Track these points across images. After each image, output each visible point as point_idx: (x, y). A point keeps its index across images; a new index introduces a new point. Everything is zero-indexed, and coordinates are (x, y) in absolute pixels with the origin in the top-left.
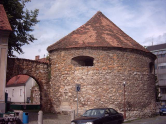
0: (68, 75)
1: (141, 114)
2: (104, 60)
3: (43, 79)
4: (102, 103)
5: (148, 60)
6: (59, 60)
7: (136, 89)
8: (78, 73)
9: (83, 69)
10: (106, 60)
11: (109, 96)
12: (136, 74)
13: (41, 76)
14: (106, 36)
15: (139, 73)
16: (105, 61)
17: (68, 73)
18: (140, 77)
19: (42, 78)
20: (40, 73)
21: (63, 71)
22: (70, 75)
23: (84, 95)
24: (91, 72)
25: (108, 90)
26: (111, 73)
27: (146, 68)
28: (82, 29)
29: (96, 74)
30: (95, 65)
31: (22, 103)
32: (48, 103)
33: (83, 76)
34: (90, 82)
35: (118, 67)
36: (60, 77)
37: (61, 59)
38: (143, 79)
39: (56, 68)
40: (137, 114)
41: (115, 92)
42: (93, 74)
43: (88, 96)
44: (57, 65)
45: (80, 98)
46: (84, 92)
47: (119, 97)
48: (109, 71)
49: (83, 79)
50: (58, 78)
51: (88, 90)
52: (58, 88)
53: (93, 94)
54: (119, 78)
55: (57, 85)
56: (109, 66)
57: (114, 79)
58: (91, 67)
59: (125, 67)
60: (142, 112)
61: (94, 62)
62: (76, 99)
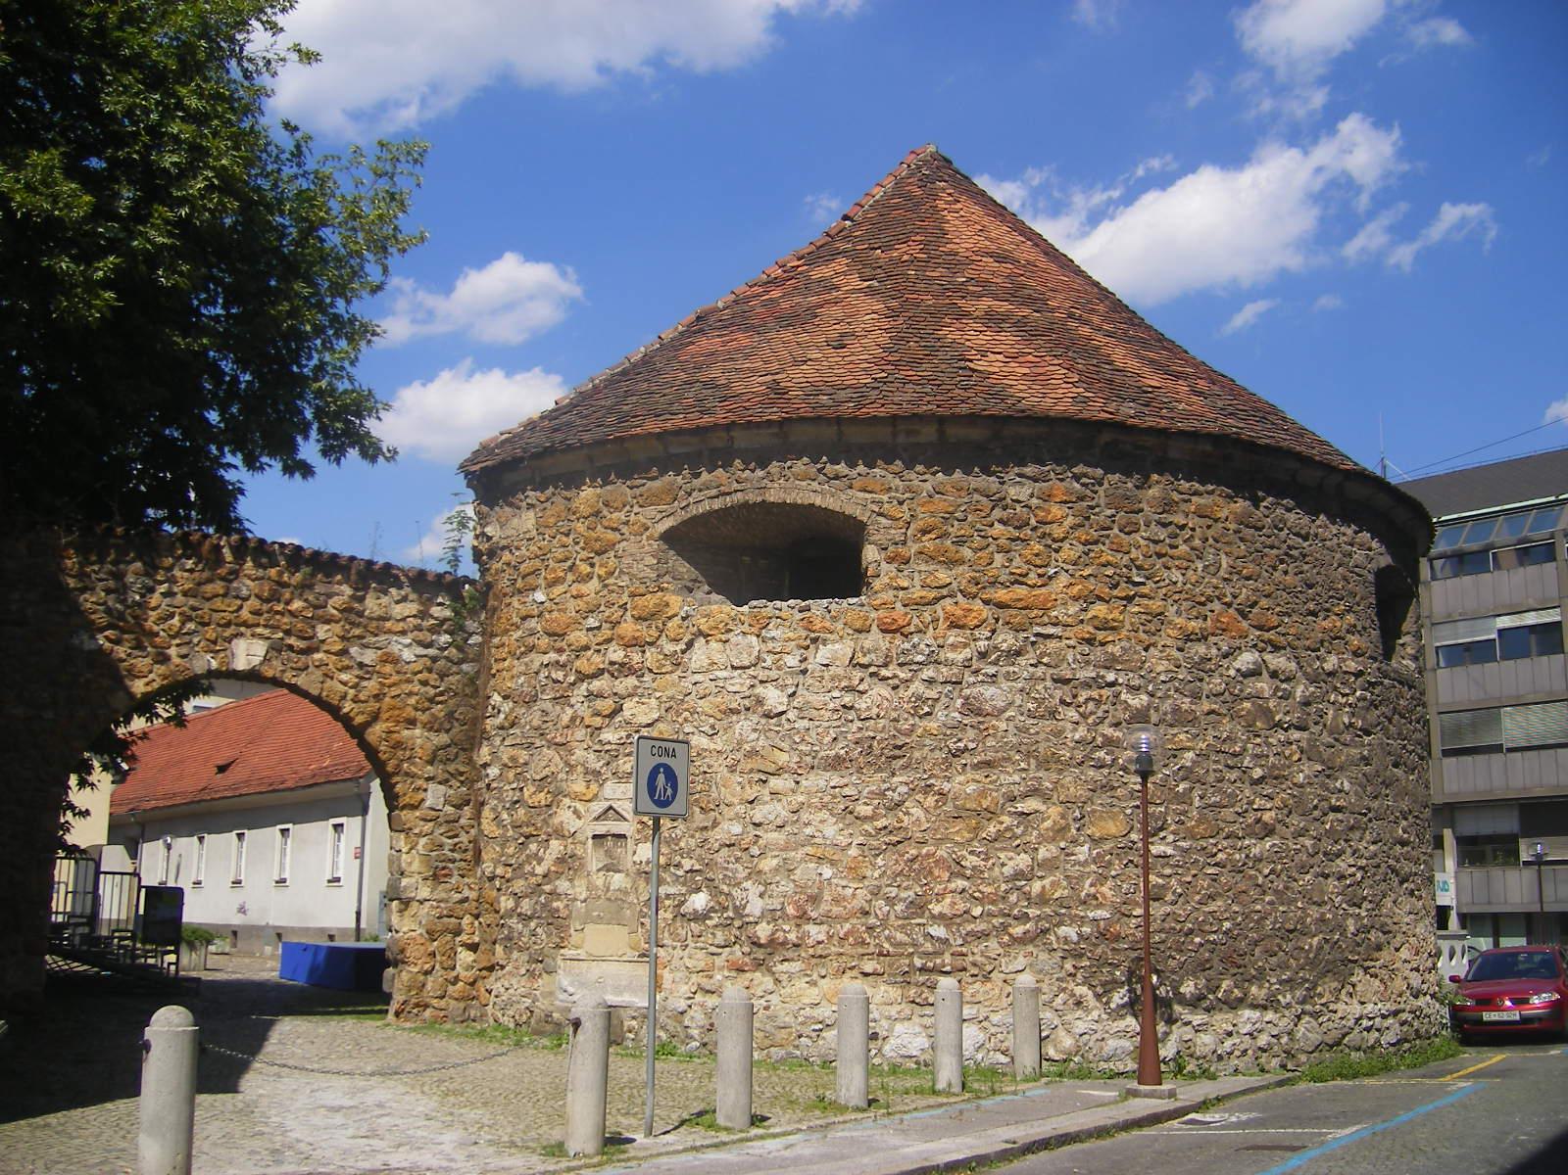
0: (632, 681)
1: (1308, 1032)
2: (960, 542)
3: (412, 723)
4: (939, 931)
5: (1370, 553)
6: (559, 553)
7: (1258, 803)
8: (719, 658)
9: (760, 627)
10: (978, 541)
11: (1007, 871)
12: (1254, 673)
13: (395, 691)
14: (976, 337)
15: (1278, 661)
16: (967, 553)
17: (636, 657)
18: (1287, 696)
19: (410, 712)
20: (388, 668)
21: (587, 648)
22: (648, 678)
23: (768, 864)
24: (836, 650)
25: (991, 814)
26: (1022, 661)
27: (1354, 621)
28: (775, 294)
29: (885, 665)
30: (877, 584)
31: (344, 931)
32: (464, 937)
33: (759, 690)
34: (824, 735)
35: (1089, 599)
36: (562, 699)
37: (569, 540)
38: (1322, 714)
39: (532, 623)
40: (1263, 1040)
41: (1060, 831)
42: (853, 663)
43: (806, 872)
44: (540, 596)
45: (736, 892)
46: (772, 837)
47: (1102, 879)
48: (1006, 640)
49: (768, 716)
50: (548, 706)
51: (805, 816)
52: (542, 798)
53: (853, 852)
54: (1098, 702)
55: (535, 772)
56: (1001, 594)
57: (1053, 714)
58: (838, 605)
59: (1155, 605)
60: (1316, 1015)
61: (870, 553)
62: (699, 901)
